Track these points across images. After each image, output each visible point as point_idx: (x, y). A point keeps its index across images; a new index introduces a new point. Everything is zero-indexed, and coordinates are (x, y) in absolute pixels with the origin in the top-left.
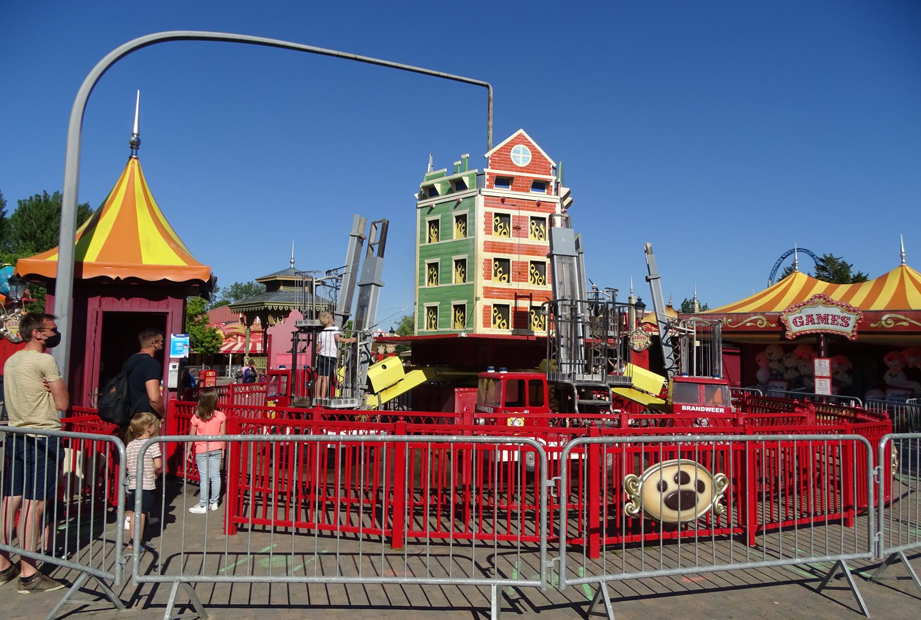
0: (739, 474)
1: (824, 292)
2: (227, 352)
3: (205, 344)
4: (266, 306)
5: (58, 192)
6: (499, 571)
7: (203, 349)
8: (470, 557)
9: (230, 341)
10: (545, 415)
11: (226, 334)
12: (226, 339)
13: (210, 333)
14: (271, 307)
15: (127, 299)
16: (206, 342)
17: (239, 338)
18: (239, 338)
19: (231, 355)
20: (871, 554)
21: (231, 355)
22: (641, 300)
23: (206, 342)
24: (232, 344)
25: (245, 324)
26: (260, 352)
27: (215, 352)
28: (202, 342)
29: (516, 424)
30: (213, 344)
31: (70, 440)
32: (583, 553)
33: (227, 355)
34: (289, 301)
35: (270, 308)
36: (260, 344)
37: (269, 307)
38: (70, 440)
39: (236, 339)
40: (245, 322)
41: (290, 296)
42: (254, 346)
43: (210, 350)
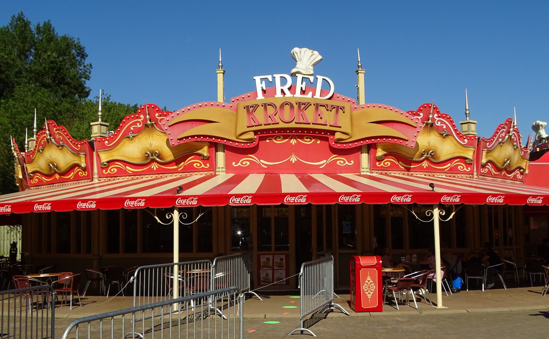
1: (289, 75)
6: (432, 303)
8: (224, 320)
9: (190, 169)
11: (174, 143)
12: (177, 162)
17: (221, 156)
18: (221, 156)
19: (176, 215)
20: (468, 277)
21: (176, 215)
22: (166, 108)
29: (12, 302)
31: (431, 292)
32: (504, 288)
38: (431, 292)
39: (210, 160)
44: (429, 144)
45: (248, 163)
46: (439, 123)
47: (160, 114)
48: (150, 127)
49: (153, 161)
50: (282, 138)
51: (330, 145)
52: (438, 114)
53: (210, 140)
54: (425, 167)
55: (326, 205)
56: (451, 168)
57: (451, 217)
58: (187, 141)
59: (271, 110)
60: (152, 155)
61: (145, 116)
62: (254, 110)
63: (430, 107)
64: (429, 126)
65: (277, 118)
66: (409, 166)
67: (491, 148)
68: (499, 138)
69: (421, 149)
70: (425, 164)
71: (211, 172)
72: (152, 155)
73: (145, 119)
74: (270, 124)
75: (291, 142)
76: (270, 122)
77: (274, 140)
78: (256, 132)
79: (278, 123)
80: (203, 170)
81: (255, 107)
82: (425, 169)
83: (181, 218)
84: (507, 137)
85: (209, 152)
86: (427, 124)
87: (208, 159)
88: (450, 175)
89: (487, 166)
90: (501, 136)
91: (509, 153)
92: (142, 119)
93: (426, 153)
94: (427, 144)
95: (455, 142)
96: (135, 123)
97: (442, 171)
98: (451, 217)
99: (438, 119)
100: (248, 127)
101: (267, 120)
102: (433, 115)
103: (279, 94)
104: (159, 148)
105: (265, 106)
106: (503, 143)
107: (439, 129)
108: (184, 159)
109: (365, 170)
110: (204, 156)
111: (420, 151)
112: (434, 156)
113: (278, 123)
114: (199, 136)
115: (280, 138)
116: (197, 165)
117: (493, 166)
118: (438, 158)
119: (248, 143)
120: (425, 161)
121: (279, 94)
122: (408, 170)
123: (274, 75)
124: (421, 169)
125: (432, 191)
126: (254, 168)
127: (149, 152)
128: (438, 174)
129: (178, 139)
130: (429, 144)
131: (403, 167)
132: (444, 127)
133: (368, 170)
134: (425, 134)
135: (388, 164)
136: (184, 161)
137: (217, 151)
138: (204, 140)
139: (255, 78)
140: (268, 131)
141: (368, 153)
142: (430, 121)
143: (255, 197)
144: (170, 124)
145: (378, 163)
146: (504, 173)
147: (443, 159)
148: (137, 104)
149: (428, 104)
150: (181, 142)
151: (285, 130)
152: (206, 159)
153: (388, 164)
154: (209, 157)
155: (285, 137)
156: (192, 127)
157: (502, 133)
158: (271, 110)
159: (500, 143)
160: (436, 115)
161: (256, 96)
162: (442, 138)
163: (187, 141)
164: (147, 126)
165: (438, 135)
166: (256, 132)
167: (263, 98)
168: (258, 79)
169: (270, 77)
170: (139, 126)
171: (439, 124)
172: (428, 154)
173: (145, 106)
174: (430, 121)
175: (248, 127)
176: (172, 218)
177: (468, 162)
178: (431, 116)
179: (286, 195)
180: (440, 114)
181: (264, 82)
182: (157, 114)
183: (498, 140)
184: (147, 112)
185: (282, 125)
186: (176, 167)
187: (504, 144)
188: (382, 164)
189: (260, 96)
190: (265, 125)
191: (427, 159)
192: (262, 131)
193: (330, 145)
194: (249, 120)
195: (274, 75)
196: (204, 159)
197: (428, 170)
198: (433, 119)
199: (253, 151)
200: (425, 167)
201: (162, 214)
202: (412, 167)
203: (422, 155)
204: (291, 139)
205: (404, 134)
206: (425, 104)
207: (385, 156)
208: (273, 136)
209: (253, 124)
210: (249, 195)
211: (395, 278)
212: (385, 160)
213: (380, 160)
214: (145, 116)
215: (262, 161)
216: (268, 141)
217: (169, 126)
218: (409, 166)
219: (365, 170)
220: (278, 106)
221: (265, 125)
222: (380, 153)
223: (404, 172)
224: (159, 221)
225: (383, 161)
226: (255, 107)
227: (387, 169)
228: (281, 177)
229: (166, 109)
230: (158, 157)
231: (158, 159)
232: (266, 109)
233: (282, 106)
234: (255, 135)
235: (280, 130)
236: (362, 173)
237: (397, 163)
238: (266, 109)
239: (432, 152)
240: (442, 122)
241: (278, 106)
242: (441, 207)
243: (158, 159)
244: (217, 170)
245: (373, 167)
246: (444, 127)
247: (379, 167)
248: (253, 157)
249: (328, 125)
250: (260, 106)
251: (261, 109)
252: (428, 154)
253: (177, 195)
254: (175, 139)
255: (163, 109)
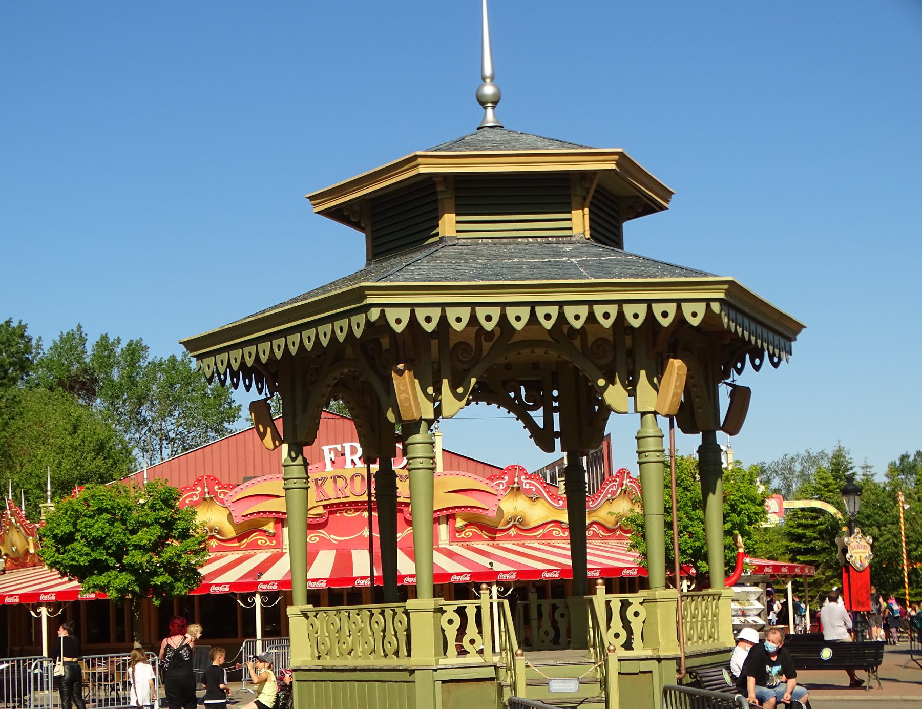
0: (827, 664)
2: (245, 589)
3: (135, 557)
4: (374, 314)
5: (102, 335)
7: (125, 579)
9: (254, 546)
10: (9, 512)
11: (239, 520)
12: (239, 538)
13: (153, 508)
14: (405, 315)
15: (625, 650)
16: (136, 547)
19: (258, 599)
21: (258, 599)
22: (81, 327)
23: (136, 547)
24: (261, 556)
25: (275, 436)
26: (367, 583)
27: (181, 589)
28: (120, 551)
30: (168, 554)
33: (244, 598)
34: (496, 276)
35: (398, 320)
36: (366, 554)
37: (391, 315)
40: (279, 425)
41: (498, 256)
42: (344, 559)
43: (158, 580)
44: (516, 510)
45: (318, 539)
46: (527, 485)
47: (220, 486)
48: (209, 501)
49: (212, 537)
50: (353, 510)
51: (405, 518)
52: (526, 476)
53: (277, 516)
54: (513, 535)
55: (343, 605)
56: (544, 534)
57: (510, 592)
58: (252, 517)
59: (340, 482)
60: (211, 532)
61: (203, 488)
62: (323, 484)
63: (516, 469)
64: (515, 490)
65: (347, 491)
66: (494, 536)
67: (595, 507)
68: (607, 492)
69: (507, 516)
70: (513, 532)
71: (278, 550)
72: (211, 532)
73: (203, 493)
74: (340, 498)
75: (363, 515)
76: (340, 495)
77: (344, 514)
78: (325, 507)
79: (349, 497)
80: (269, 547)
81: (324, 480)
82: (512, 537)
83: (262, 601)
84: (619, 491)
85: (275, 528)
86: (513, 488)
87: (274, 536)
88: (543, 541)
89: (591, 528)
90: (610, 491)
91: (623, 511)
92: (198, 492)
93: (513, 520)
94: (513, 510)
95: (547, 505)
96: (191, 496)
97: (534, 538)
98: (510, 592)
99: (525, 481)
100: (317, 502)
101: (337, 494)
102: (519, 477)
103: (349, 465)
104: (219, 524)
105: (334, 478)
106: (613, 500)
107: (527, 492)
108: (247, 535)
109: (444, 542)
110: (269, 533)
111: (505, 518)
112: (523, 522)
113: (349, 497)
114: (265, 512)
115: (351, 511)
116: (261, 542)
117: (601, 527)
118: (528, 524)
119: (316, 518)
120: (513, 528)
121: (349, 465)
122: (493, 539)
123: (344, 445)
124: (509, 538)
125: (489, 569)
126: (325, 544)
127: (208, 528)
128: (529, 542)
129: (243, 516)
130: (516, 510)
131: (487, 536)
132: (534, 489)
133: (448, 542)
134: (511, 500)
135: (469, 535)
136: (247, 537)
137: (283, 527)
138: (271, 516)
139: (323, 448)
140: (338, 504)
141: (447, 523)
142: (516, 485)
143: (329, 581)
144: (233, 501)
145: (457, 534)
146: (618, 533)
147: (532, 526)
148: (11, 318)
149: (512, 466)
150: (246, 519)
151: (356, 503)
152: (272, 536)
153: (469, 535)
154: (275, 533)
155: (356, 510)
156: (257, 503)
157: (612, 487)
158: (340, 482)
159: (608, 500)
160: (523, 477)
161: (325, 467)
162: (531, 502)
163: (252, 517)
164: (205, 499)
165: (527, 499)
166: (325, 507)
167: (332, 469)
168: (326, 449)
169: (339, 447)
170: (195, 498)
171: (527, 487)
172: (515, 521)
173: (202, 477)
174: (516, 485)
175: (317, 502)
176: (254, 601)
177: (564, 527)
178: (516, 480)
179: (356, 578)
180: (528, 475)
181: (332, 452)
182: (216, 487)
183: (606, 495)
184: (206, 485)
185: (353, 498)
186: (238, 544)
187: (615, 501)
188: (463, 535)
189: (329, 467)
190: (334, 499)
191: (514, 526)
192: (332, 505)
193: (405, 518)
194: (318, 495)
195: (344, 445)
196: (269, 536)
197: (517, 537)
198: (520, 482)
199: (323, 525)
200: (513, 535)
201: (244, 598)
202: (497, 536)
203: (509, 522)
204: (363, 511)
205: (483, 503)
206: (510, 466)
207: (466, 526)
208: (343, 510)
209: (322, 498)
210: (324, 579)
211: (182, 540)
212: (466, 530)
213: (460, 531)
214: (203, 488)
215: (332, 536)
216: (338, 515)
217: (233, 502)
218: (494, 536)
219: (444, 542)
220: (348, 478)
221: (334, 499)
222: (459, 523)
223: (488, 542)
224: (241, 604)
225: (464, 532)
226: (324, 480)
227: (469, 540)
228: (353, 554)
229: (82, 329)
230: (218, 533)
231: (218, 536)
232: (335, 481)
233: (353, 478)
234: (324, 509)
235: (350, 503)
236: (440, 546)
237: (480, 533)
238: (335, 481)
239: (520, 518)
240: (531, 484)
241: (348, 478)
242: (499, 584)
243: (218, 536)
244: (284, 547)
245: (453, 539)
246: (534, 490)
247: (459, 538)
248: (323, 533)
249: (402, 497)
250: (329, 478)
251: (330, 482)
252: (515, 521)
253: (258, 580)
254: (239, 516)
255: (75, 330)
